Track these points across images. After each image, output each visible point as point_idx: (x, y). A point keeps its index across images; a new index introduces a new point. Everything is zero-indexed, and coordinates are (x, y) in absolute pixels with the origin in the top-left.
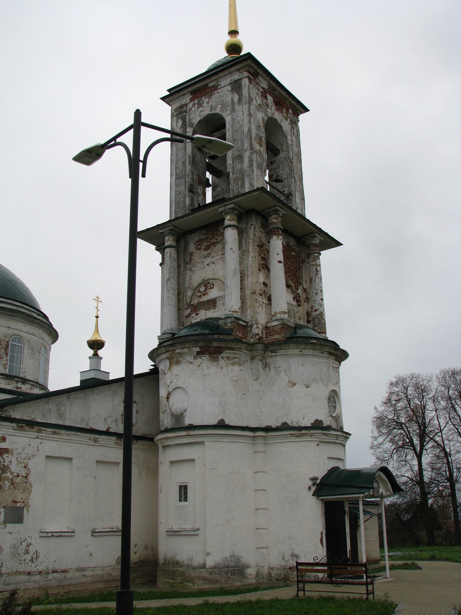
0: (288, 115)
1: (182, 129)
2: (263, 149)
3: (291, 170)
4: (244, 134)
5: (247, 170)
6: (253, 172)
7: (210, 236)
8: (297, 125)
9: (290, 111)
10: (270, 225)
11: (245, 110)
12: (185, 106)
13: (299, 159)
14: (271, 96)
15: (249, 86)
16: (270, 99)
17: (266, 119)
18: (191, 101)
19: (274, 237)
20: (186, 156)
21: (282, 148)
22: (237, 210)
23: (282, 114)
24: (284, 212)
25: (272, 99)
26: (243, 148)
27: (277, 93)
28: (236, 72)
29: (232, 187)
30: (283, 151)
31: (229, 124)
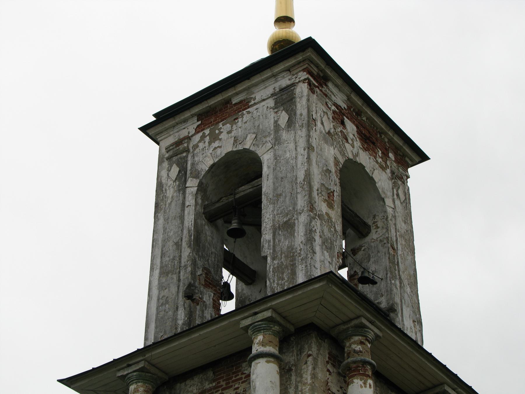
0: (386, 163)
1: (177, 183)
2: (336, 215)
3: (393, 263)
4: (296, 183)
5: (301, 250)
6: (314, 253)
7: (223, 383)
8: (404, 183)
9: (391, 155)
10: (349, 357)
11: (301, 140)
12: (186, 141)
13: (409, 245)
14: (353, 123)
15: (308, 96)
16: (351, 127)
17: (342, 160)
18: (198, 132)
19: (355, 381)
20: (182, 231)
21: (374, 223)
22: (280, 324)
23: (375, 157)
24: (377, 331)
25: (355, 128)
26: (294, 208)
27: (364, 119)
28: (284, 74)
29: (271, 283)
30: (377, 227)
31: (269, 167)
